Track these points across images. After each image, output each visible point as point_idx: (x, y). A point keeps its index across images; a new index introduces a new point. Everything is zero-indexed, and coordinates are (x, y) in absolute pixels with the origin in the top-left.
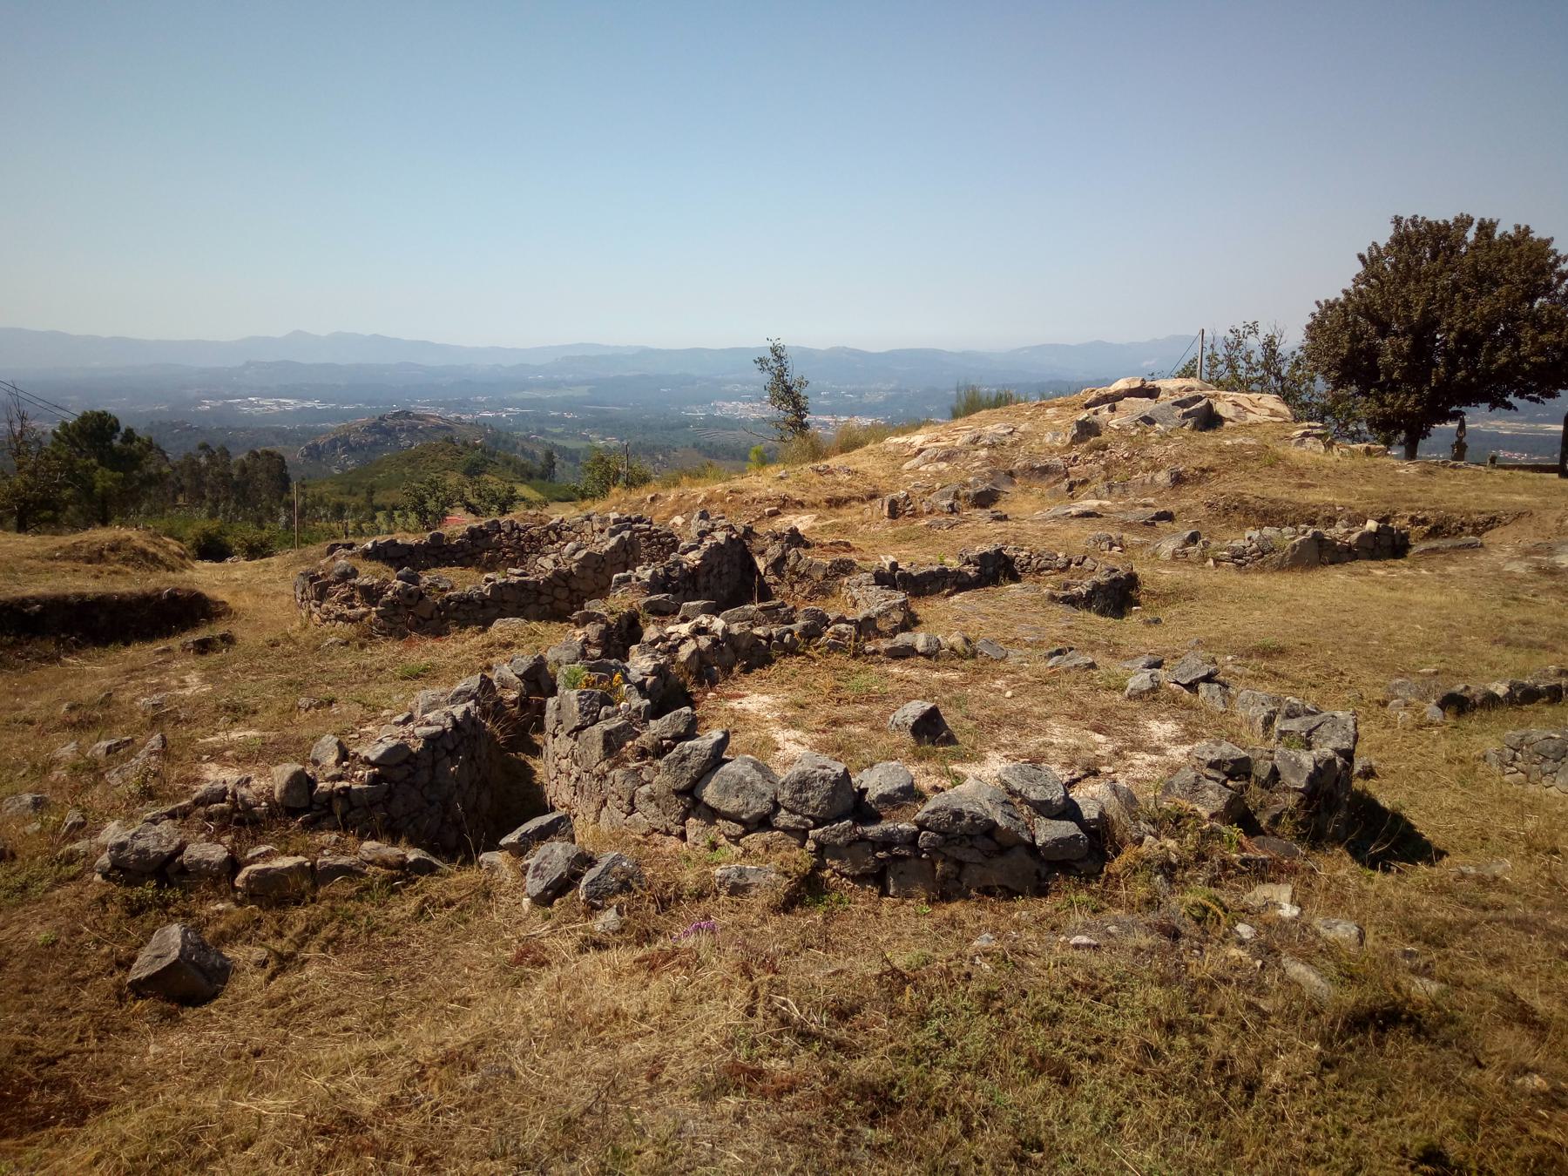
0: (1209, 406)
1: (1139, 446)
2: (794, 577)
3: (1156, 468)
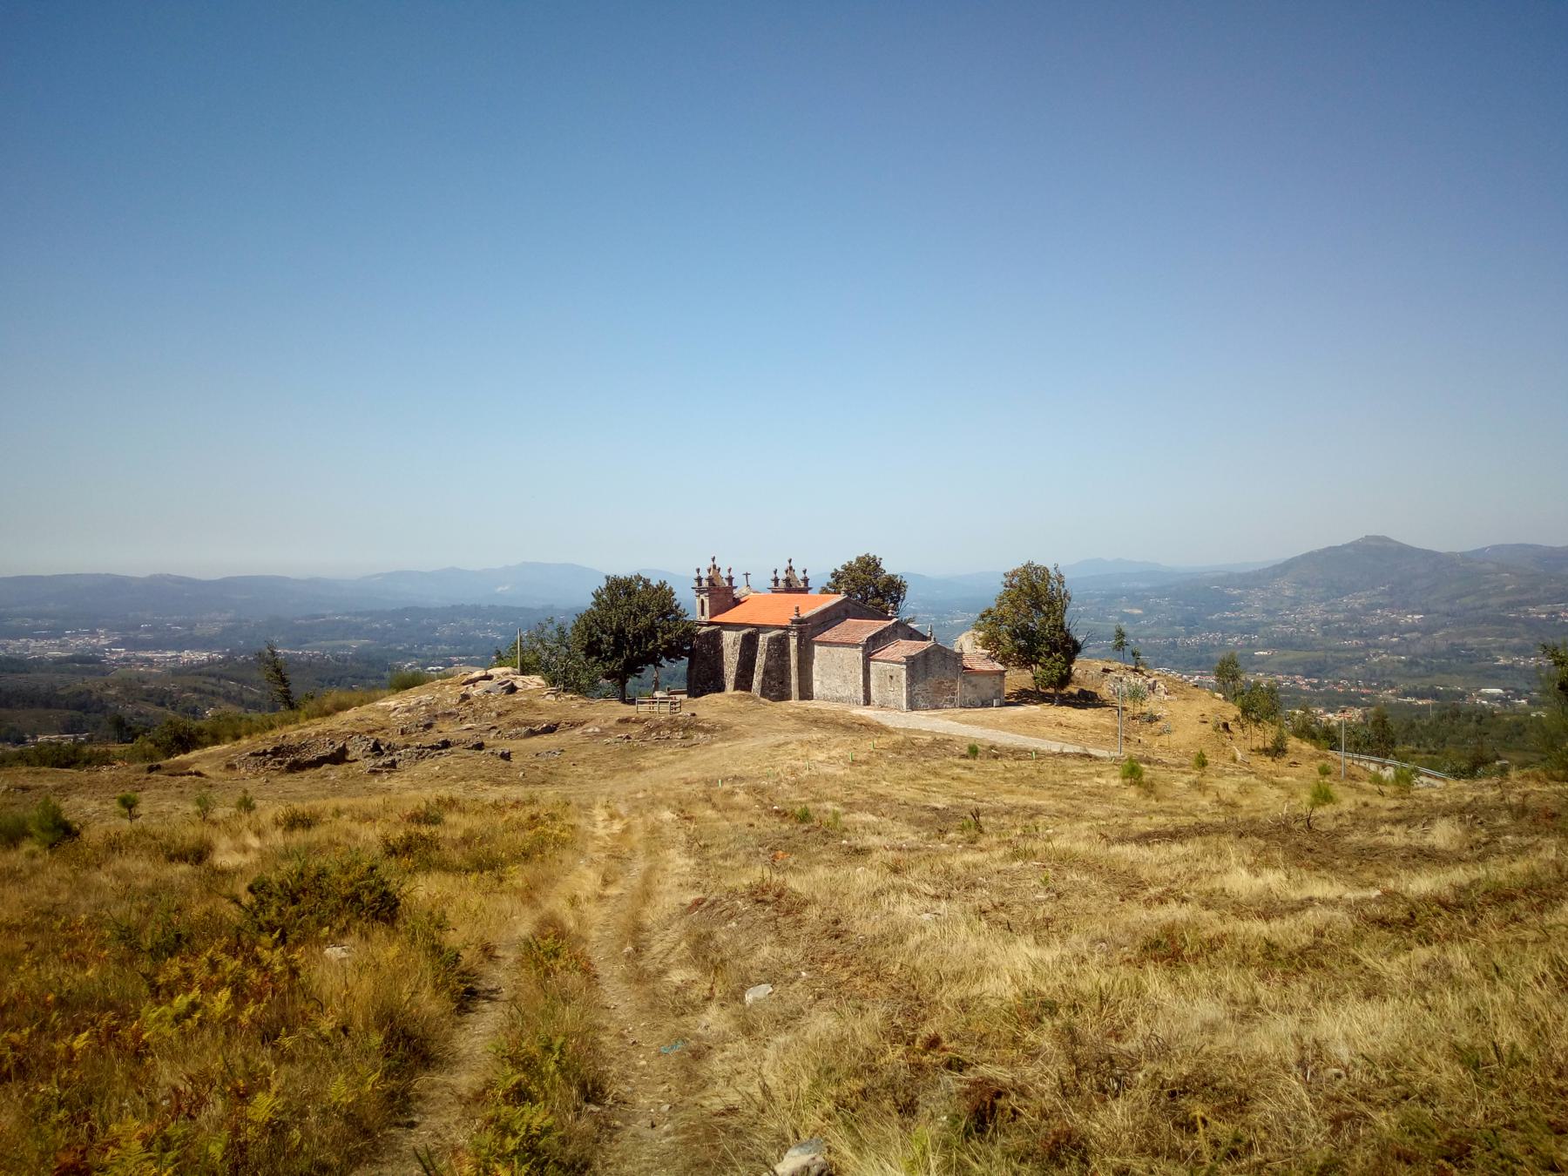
0: (512, 684)
1: (485, 702)
3: (491, 711)
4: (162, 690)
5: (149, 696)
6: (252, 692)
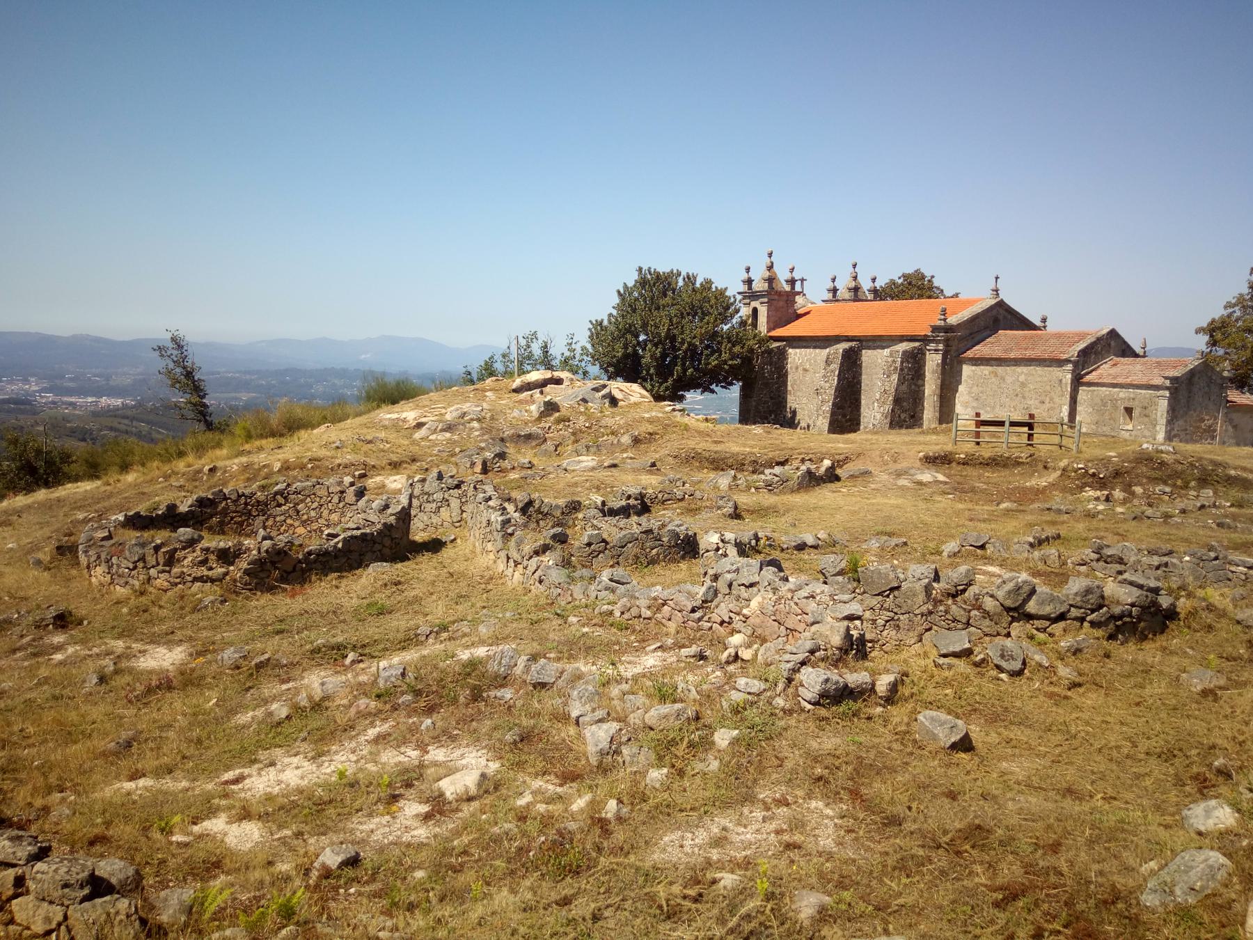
2: (540, 516)
4: (84, 428)
5: (72, 433)
6: (159, 432)
